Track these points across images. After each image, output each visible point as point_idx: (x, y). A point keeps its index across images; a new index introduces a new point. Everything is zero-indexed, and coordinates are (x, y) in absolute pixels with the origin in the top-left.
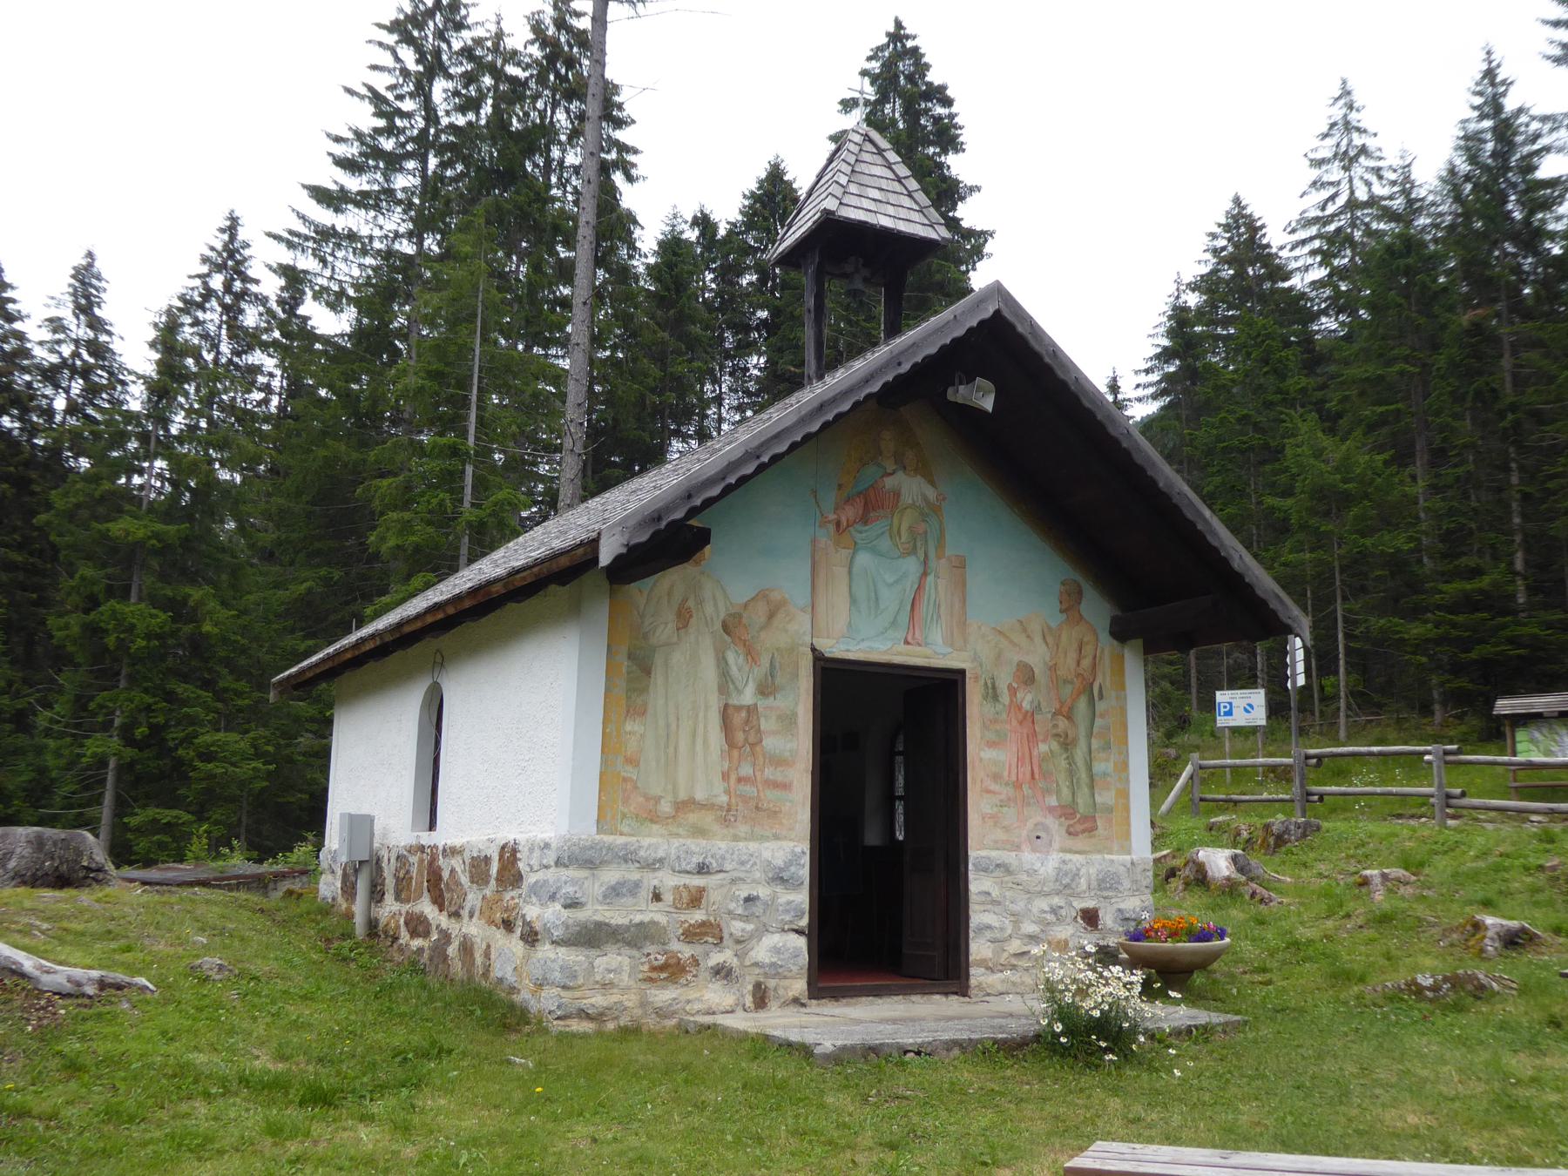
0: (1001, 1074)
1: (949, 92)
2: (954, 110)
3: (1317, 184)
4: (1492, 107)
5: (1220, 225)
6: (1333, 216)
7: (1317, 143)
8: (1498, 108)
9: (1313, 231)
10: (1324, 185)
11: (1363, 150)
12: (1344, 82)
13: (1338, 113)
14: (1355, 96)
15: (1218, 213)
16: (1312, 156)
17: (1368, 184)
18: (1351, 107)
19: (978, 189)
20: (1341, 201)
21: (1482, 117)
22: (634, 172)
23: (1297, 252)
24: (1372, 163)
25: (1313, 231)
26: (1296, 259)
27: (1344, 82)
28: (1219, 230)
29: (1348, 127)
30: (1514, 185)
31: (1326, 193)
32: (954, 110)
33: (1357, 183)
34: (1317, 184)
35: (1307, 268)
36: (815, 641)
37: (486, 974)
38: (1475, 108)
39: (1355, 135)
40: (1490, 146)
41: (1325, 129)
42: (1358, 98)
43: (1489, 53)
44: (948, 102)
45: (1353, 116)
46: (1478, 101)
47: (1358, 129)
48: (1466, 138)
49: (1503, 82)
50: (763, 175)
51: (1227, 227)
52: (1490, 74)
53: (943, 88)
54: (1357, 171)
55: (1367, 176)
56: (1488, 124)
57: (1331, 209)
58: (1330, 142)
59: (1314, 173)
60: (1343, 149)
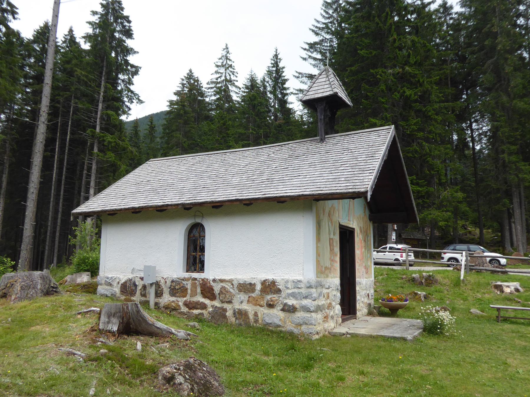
0: (321, 335)
1: (130, 19)
2: (131, 25)
3: (217, 72)
4: (276, 64)
5: (185, 77)
6: (220, 82)
7: (218, 60)
8: (278, 66)
9: (213, 86)
10: (219, 73)
11: (231, 66)
12: (227, 45)
13: (224, 53)
14: (229, 50)
15: (184, 73)
16: (217, 64)
17: (230, 75)
18: (228, 52)
19: (138, 53)
20: (223, 78)
21: (273, 67)
22: (16, 16)
23: (209, 90)
24: (232, 70)
25: (213, 86)
26: (209, 92)
27: (227, 45)
28: (184, 78)
29: (227, 58)
30: (279, 87)
31: (218, 75)
32: (131, 25)
33: (227, 75)
34: (217, 72)
35: (211, 96)
36: (340, 220)
37: (256, 321)
38: (272, 64)
39: (228, 61)
40: (274, 75)
41: (220, 57)
42: (230, 50)
43: (276, 50)
44: (129, 22)
45: (228, 55)
46: (273, 62)
47: (229, 60)
48: (268, 71)
49: (280, 59)
50: (42, 25)
51: (187, 78)
52: (276, 56)
53: (127, 17)
54: (228, 71)
55: (230, 73)
56: (274, 69)
57: (219, 80)
58: (221, 61)
59: (216, 69)
60: (224, 64)
